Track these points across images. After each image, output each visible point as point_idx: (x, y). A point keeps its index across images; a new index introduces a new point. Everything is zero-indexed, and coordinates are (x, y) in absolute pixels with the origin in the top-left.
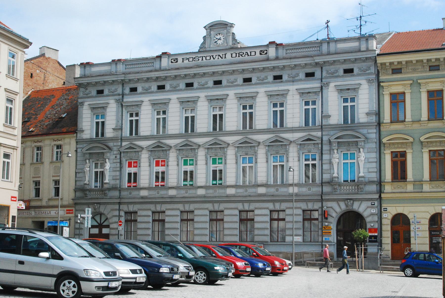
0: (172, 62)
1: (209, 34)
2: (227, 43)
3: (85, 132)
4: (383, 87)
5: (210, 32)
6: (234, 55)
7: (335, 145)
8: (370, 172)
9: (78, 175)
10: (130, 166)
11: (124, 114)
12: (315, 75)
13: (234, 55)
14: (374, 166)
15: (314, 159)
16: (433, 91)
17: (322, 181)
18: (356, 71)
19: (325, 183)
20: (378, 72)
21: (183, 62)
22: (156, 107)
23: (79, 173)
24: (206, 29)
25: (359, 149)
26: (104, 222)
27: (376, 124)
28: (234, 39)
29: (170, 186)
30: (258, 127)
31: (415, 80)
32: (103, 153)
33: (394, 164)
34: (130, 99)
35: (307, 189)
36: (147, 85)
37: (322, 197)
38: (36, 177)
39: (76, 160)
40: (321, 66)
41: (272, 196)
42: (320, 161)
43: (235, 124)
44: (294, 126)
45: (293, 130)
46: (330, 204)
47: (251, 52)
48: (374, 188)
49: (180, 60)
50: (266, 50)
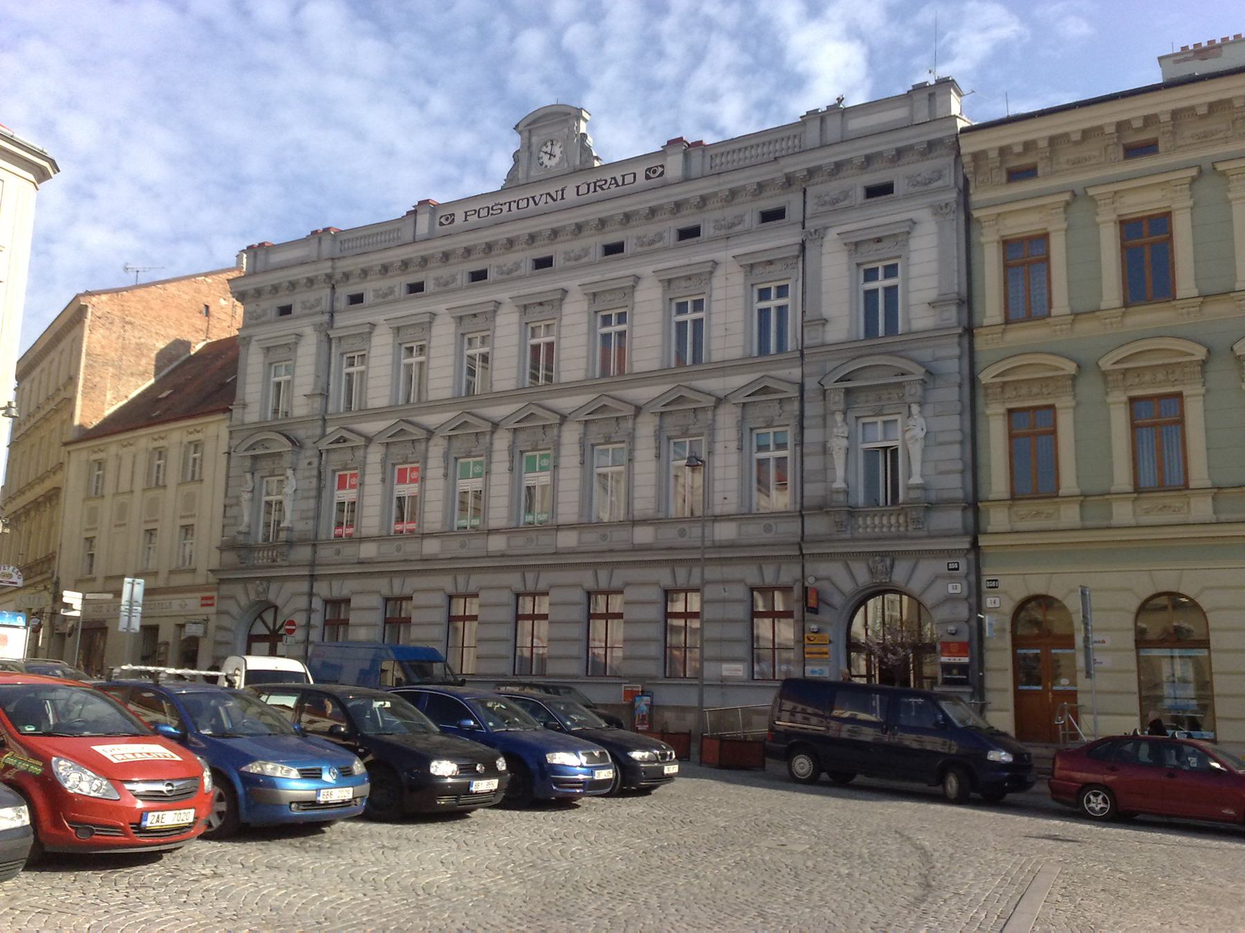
0: (441, 224)
1: (527, 146)
4: (978, 220)
7: (837, 400)
8: (941, 473)
12: (895, 187)
13: (583, 189)
14: (954, 453)
15: (781, 446)
16: (1139, 221)
17: (802, 504)
18: (900, 187)
19: (810, 509)
23: (231, 506)
24: (520, 133)
26: (275, 625)
28: (586, 150)
29: (363, 535)
30: (637, 367)
31: (1079, 191)
34: (349, 319)
37: (801, 549)
38: (188, 517)
39: (228, 477)
41: (503, 556)
42: (798, 448)
44: (727, 357)
45: (724, 368)
46: (824, 569)
48: (954, 519)
49: (459, 218)
50: (662, 166)
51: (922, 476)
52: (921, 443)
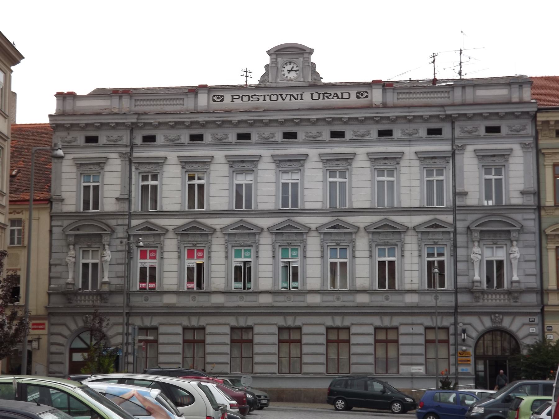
0: (214, 101)
2: (304, 77)
3: (67, 201)
5: (276, 59)
6: (316, 96)
9: (53, 269)
10: (143, 256)
11: (133, 176)
12: (251, 137)
13: (316, 96)
14: (533, 268)
15: (442, 255)
19: (461, 289)
20: (537, 132)
21: (232, 101)
22: (188, 167)
23: (56, 265)
25: (104, 245)
27: (535, 207)
32: (100, 236)
35: (384, 297)
36: (172, 134)
39: (51, 245)
40: (451, 119)
43: (320, 198)
46: (468, 319)
47: (342, 93)
49: (228, 98)
51: (518, 276)
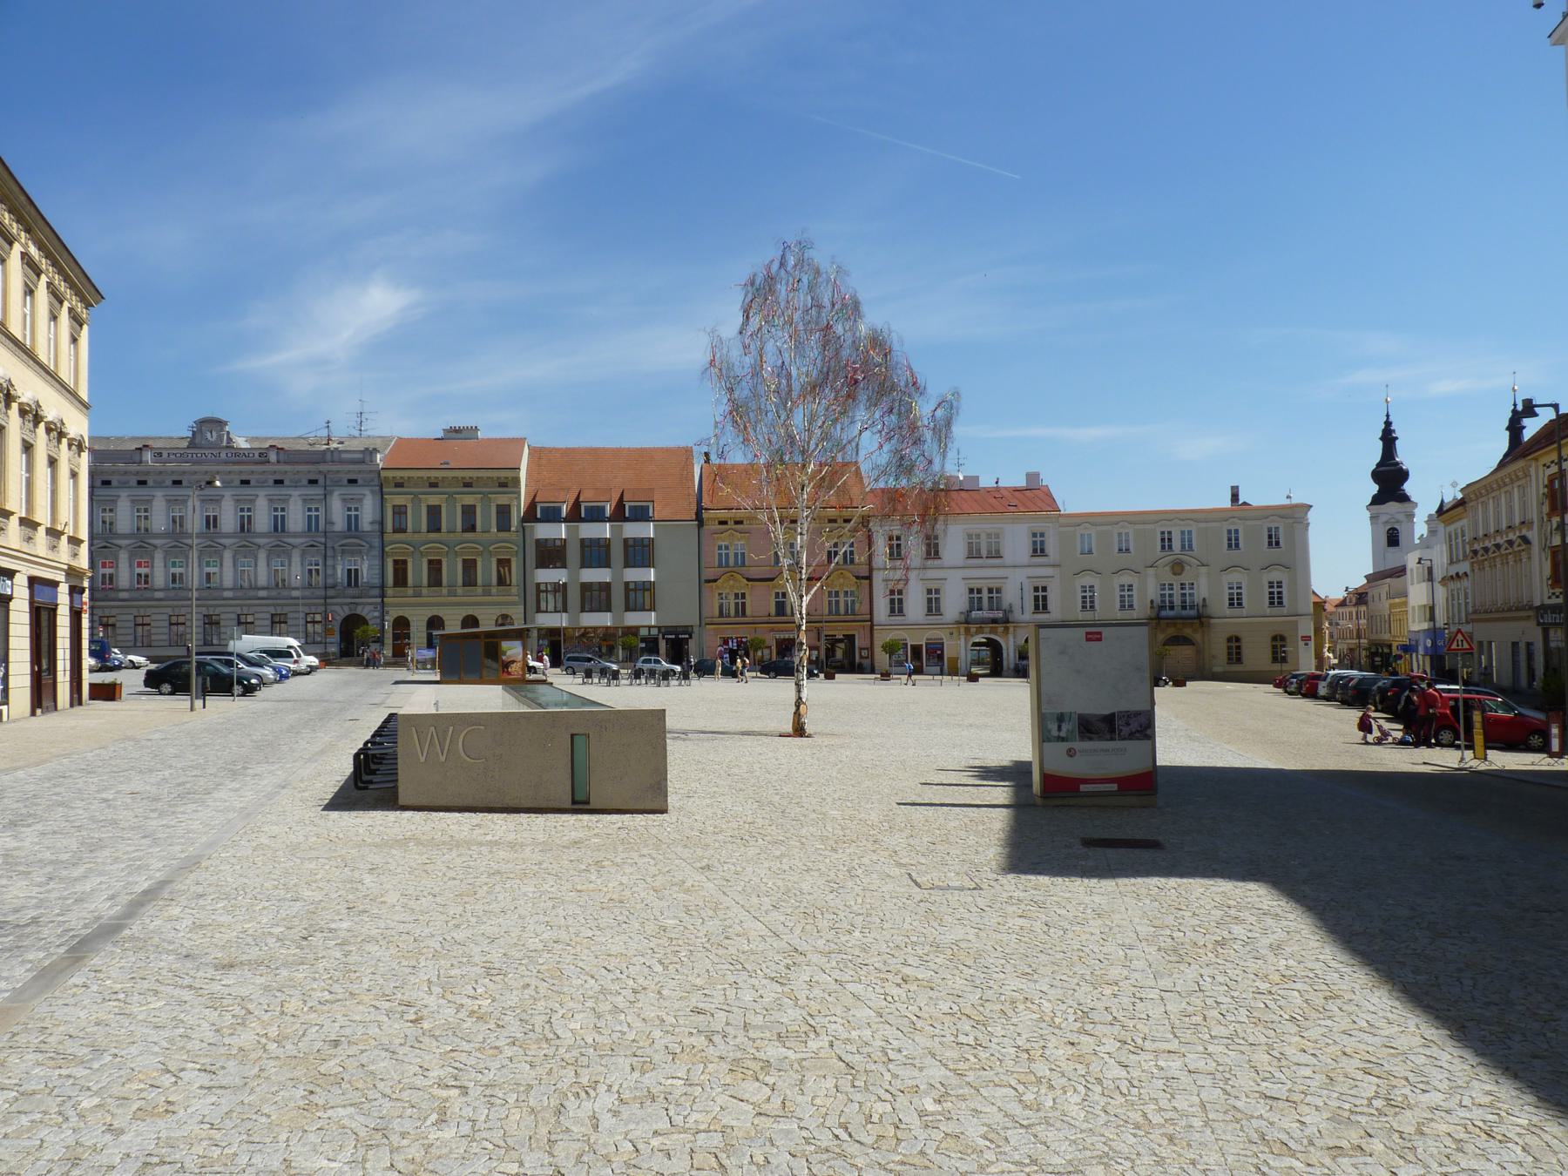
14: (377, 571)
33: (395, 570)
48: (376, 592)
52: (367, 569)
